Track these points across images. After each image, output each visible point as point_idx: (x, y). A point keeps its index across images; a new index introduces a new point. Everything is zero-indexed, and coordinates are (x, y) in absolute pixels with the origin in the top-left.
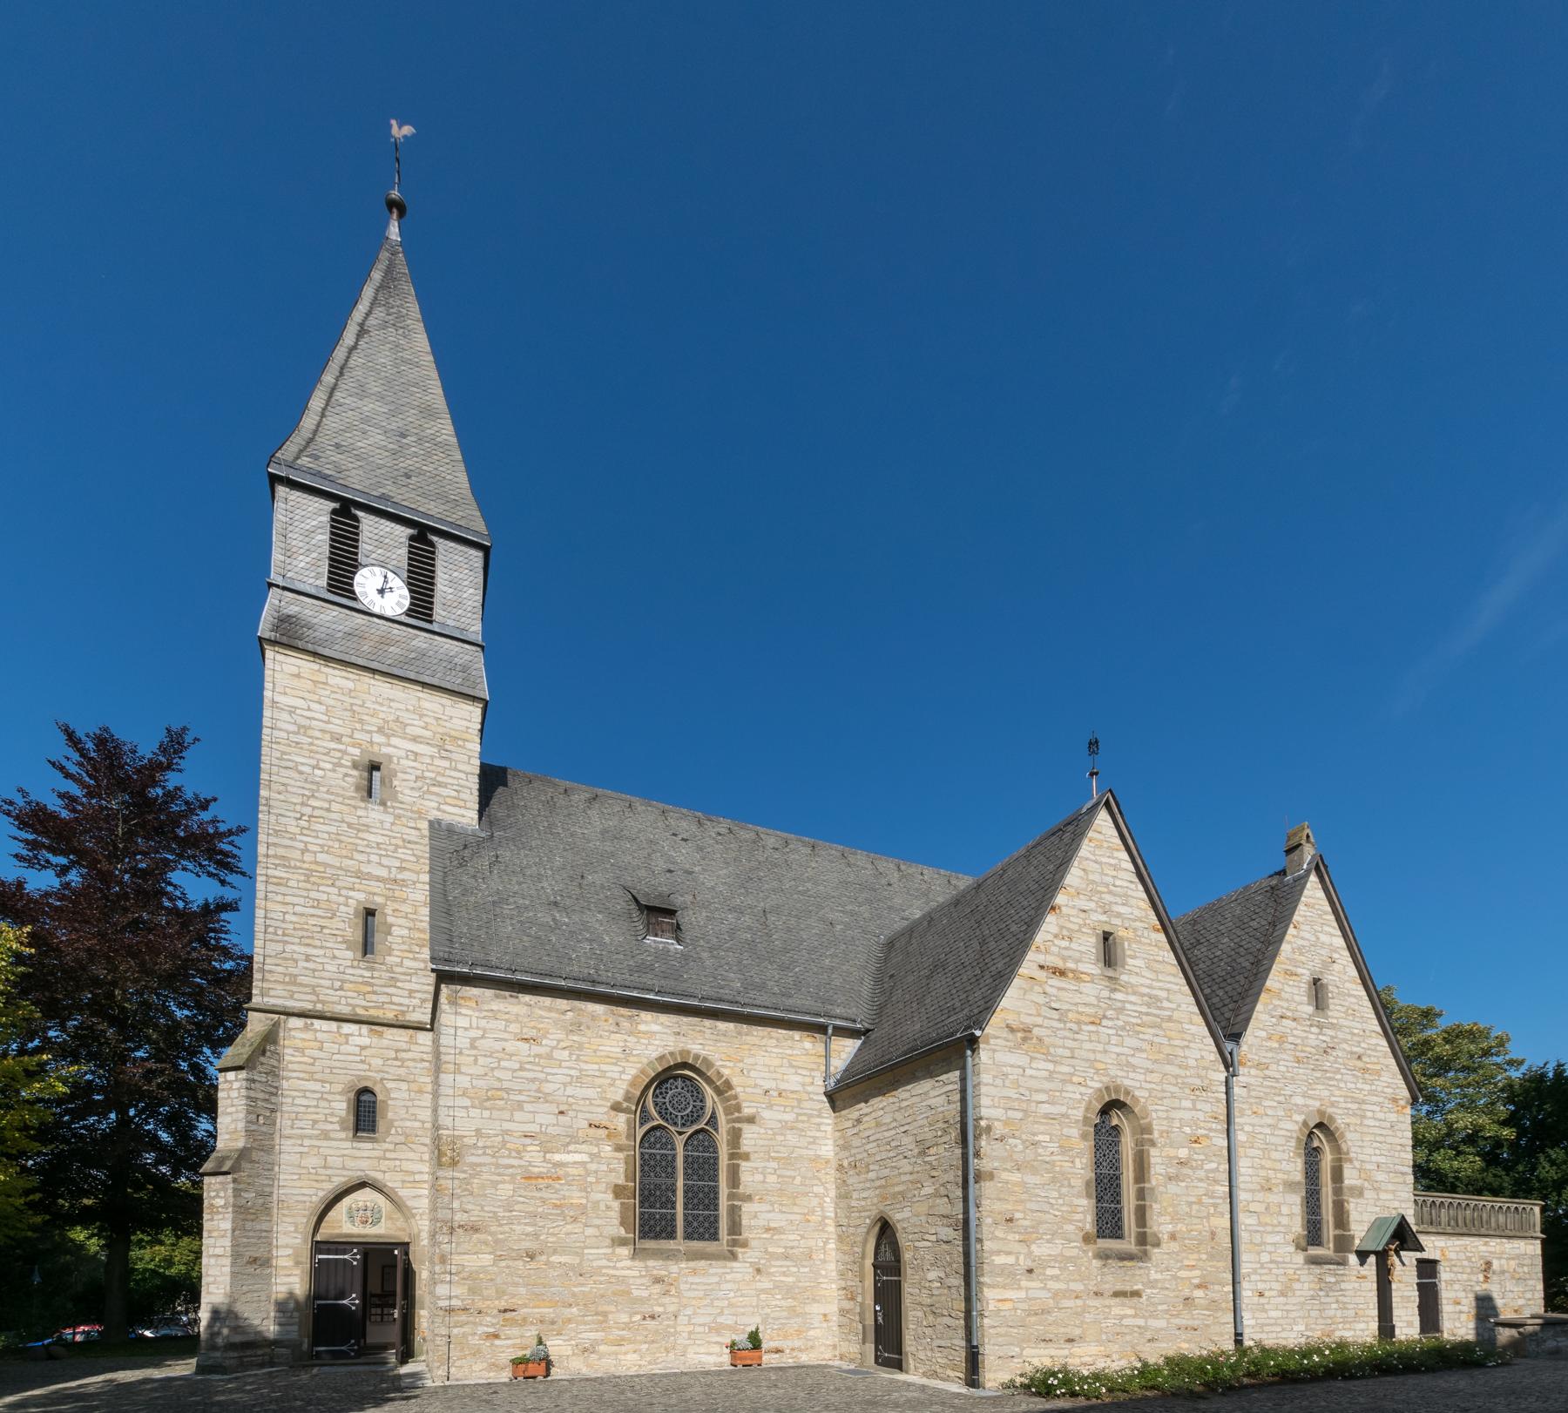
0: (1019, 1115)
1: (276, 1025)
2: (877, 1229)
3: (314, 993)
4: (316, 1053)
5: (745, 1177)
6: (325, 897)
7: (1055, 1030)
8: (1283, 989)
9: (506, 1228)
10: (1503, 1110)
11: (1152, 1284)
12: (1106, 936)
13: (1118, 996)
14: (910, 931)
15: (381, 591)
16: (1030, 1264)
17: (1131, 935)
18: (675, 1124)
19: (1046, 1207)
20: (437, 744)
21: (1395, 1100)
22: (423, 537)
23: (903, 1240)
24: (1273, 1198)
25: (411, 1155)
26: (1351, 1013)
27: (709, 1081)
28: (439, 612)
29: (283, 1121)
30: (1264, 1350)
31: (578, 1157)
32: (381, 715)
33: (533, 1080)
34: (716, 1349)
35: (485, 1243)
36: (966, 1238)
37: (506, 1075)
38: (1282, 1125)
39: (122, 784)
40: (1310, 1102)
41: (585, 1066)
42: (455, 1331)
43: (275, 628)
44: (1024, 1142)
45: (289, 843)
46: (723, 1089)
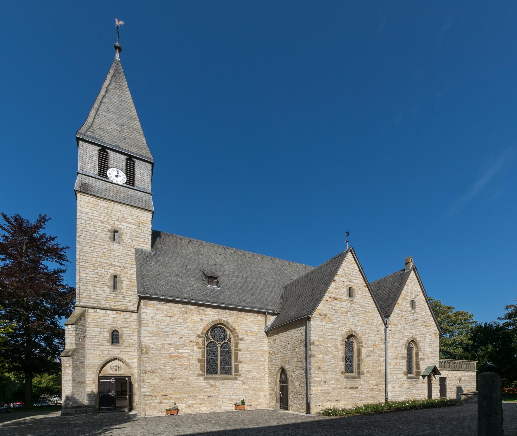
0: (323, 339)
1: (85, 311)
2: (281, 371)
3: (97, 301)
4: (98, 320)
5: (240, 356)
6: (100, 272)
7: (334, 315)
8: (402, 303)
9: (164, 372)
10: (469, 336)
11: (362, 385)
12: (350, 289)
13: (353, 305)
14: (292, 284)
15: (117, 176)
16: (325, 380)
17: (357, 288)
18: (218, 341)
19: (330, 364)
20: (137, 225)
21: (435, 334)
22: (131, 159)
23: (288, 374)
24: (397, 361)
25: (131, 350)
26: (423, 310)
27: (228, 328)
28: (136, 183)
29: (88, 340)
30: (392, 402)
31: (186, 351)
32: (118, 215)
33: (172, 328)
34: (231, 405)
35: (157, 376)
36: (306, 373)
37: (163, 327)
38: (401, 341)
39: (25, 233)
40: (409, 335)
41: (188, 324)
42: (148, 402)
43: (80, 187)
44: (324, 346)
45: (87, 255)
46: (233, 331)
